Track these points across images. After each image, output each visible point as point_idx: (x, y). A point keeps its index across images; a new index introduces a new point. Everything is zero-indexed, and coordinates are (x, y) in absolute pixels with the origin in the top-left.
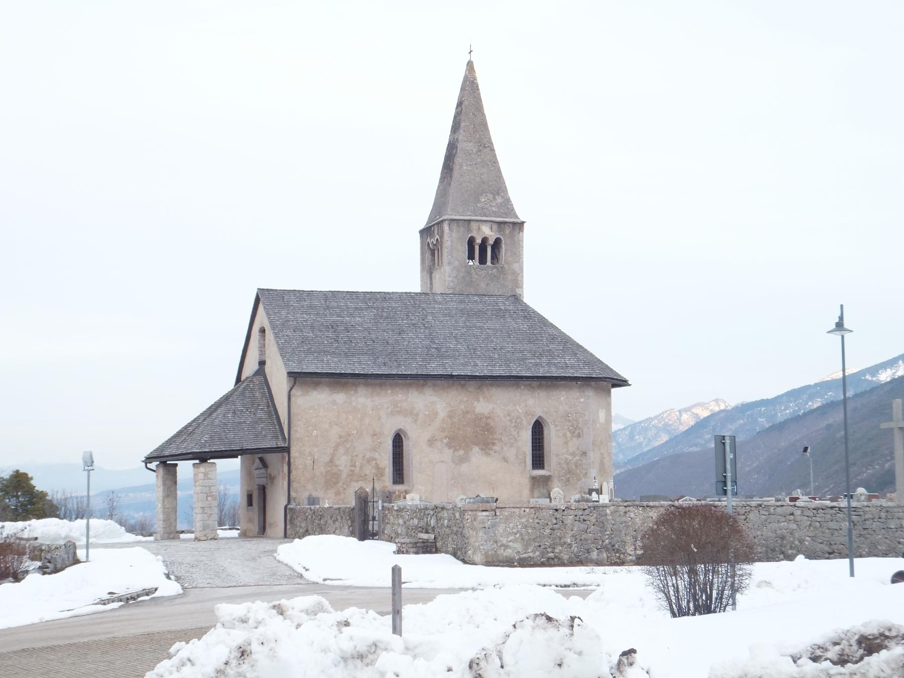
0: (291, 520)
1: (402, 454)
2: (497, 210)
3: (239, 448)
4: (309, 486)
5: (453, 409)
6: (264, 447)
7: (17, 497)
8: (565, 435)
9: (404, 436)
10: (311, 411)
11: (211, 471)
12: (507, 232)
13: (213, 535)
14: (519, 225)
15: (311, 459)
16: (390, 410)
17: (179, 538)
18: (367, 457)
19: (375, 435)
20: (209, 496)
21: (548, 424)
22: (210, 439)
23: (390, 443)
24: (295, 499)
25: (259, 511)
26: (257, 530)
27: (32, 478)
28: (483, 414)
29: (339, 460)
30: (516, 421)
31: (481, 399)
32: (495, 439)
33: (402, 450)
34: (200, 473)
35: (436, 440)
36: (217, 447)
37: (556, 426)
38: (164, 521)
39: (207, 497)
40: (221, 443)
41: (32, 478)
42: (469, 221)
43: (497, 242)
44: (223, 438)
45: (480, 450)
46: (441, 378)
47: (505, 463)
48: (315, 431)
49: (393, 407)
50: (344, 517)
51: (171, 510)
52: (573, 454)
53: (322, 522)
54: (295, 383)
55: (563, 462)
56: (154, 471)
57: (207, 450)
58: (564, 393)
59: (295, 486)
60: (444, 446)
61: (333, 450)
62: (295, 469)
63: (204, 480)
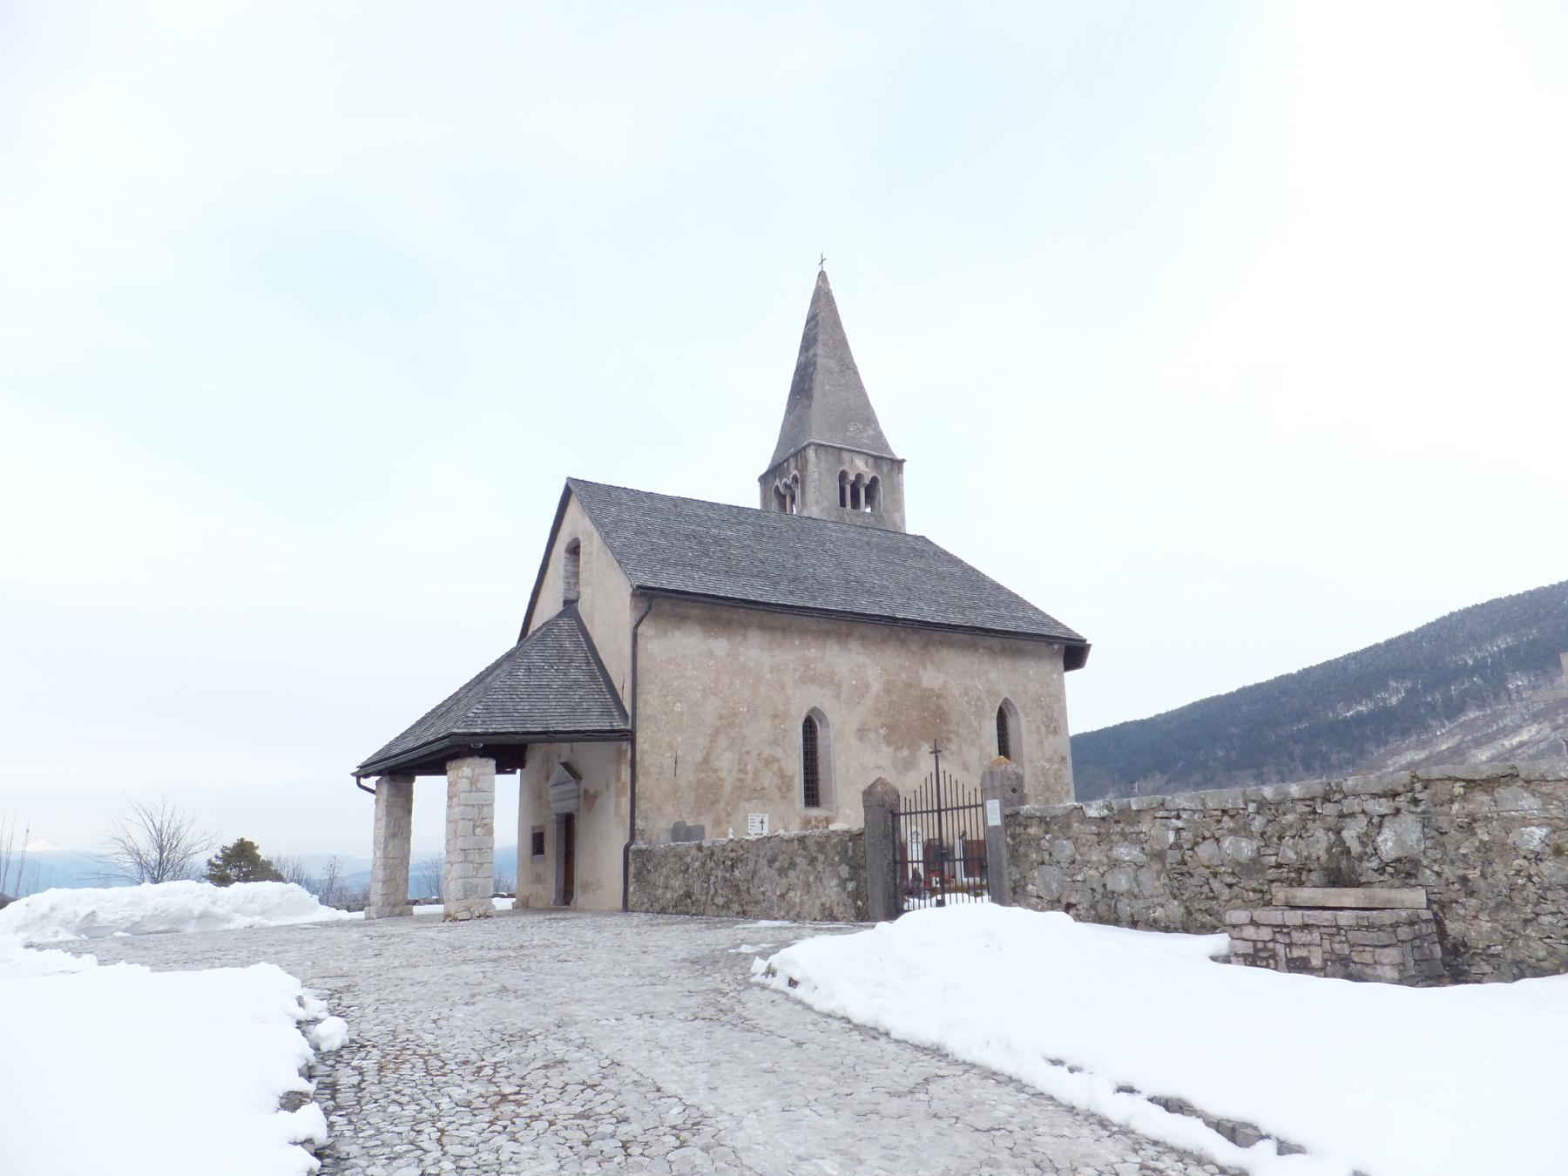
0: (639, 873)
1: (816, 752)
2: (870, 443)
3: (540, 729)
4: (669, 809)
5: (891, 678)
6: (588, 728)
7: (240, 868)
9: (820, 721)
10: (671, 667)
11: (484, 774)
12: (885, 470)
13: (484, 907)
14: (898, 464)
15: (671, 757)
17: (412, 914)
18: (765, 755)
19: (776, 716)
20: (478, 826)
21: (1016, 713)
22: (484, 711)
23: (800, 730)
24: (642, 832)
25: (557, 861)
26: (554, 896)
27: (257, 847)
30: (976, 705)
31: (929, 666)
32: (951, 732)
33: (815, 746)
34: (462, 777)
35: (869, 730)
36: (499, 727)
37: (1027, 715)
38: (384, 882)
39: (475, 827)
40: (506, 718)
41: (257, 847)
42: (841, 449)
43: (874, 480)
44: (510, 711)
46: (880, 621)
47: (966, 772)
48: (678, 704)
49: (803, 668)
50: (821, 858)
51: (399, 861)
52: (1050, 760)
53: (737, 873)
54: (650, 607)
56: (372, 792)
57: (478, 731)
58: (1032, 664)
59: (643, 807)
60: (881, 741)
61: (708, 740)
63: (469, 792)
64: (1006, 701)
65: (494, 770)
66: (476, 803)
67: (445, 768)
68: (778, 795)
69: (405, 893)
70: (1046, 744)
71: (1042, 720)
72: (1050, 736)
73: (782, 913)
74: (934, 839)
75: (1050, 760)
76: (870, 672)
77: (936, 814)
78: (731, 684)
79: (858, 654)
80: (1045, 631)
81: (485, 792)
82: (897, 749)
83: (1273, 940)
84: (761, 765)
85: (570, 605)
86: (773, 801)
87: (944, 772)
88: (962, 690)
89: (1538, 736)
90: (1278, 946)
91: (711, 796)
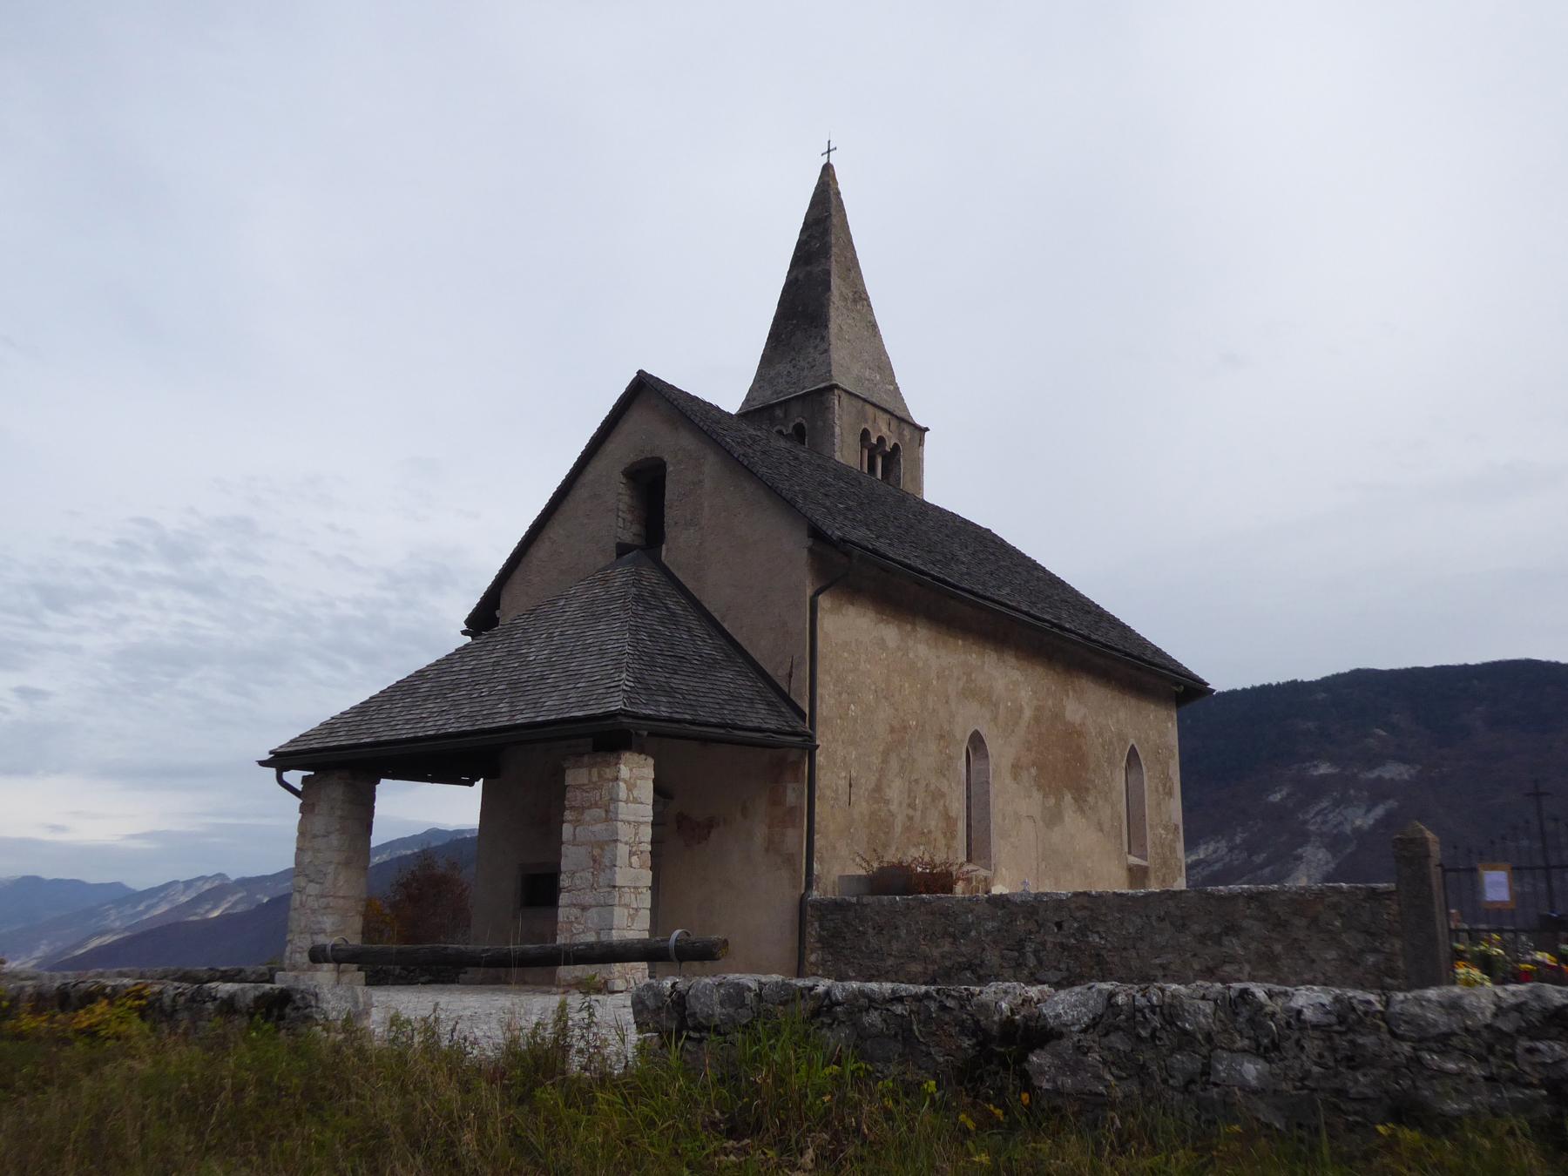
15: (845, 777)
19: (942, 737)
20: (634, 854)
31: (1071, 693)
61: (880, 760)
75: (1166, 827)
76: (1023, 693)
81: (642, 803)
89: (1214, 856)
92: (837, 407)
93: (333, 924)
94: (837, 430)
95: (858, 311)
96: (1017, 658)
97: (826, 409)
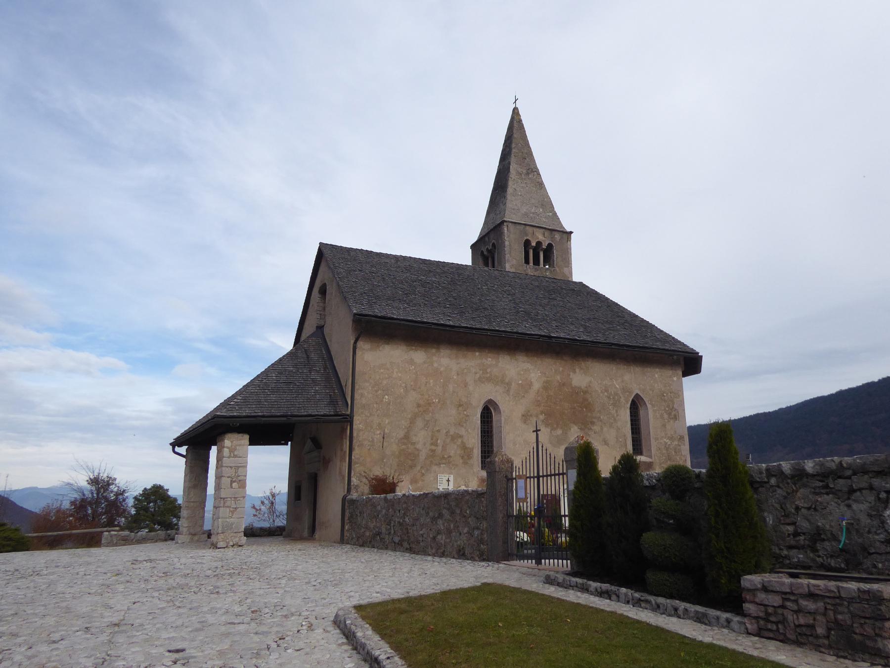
0: (351, 517)
8: (662, 416)
9: (494, 409)
10: (382, 371)
11: (240, 445)
15: (380, 433)
16: (478, 376)
18: (452, 433)
19: (460, 405)
20: (234, 482)
28: (580, 388)
29: (415, 435)
30: (614, 398)
31: (577, 370)
37: (653, 406)
39: (232, 482)
43: (550, 246)
45: (579, 430)
47: (606, 446)
48: (386, 397)
52: (671, 438)
55: (663, 447)
57: (235, 414)
58: (657, 370)
62: (358, 446)
64: (637, 396)
65: (248, 443)
66: (233, 465)
67: (216, 440)
68: (461, 461)
69: (202, 526)
70: (668, 427)
71: (665, 409)
72: (672, 421)
73: (434, 551)
74: (547, 495)
75: (671, 438)
76: (532, 375)
77: (536, 479)
78: (426, 382)
79: (524, 362)
80: (618, 336)
82: (553, 429)
83: (783, 607)
84: (448, 440)
85: (320, 328)
86: (457, 465)
87: (546, 450)
88: (603, 388)
90: (786, 612)
91: (410, 462)
92: (506, 232)
93: (188, 514)
94: (507, 243)
95: (530, 179)
96: (527, 356)
97: (501, 234)
